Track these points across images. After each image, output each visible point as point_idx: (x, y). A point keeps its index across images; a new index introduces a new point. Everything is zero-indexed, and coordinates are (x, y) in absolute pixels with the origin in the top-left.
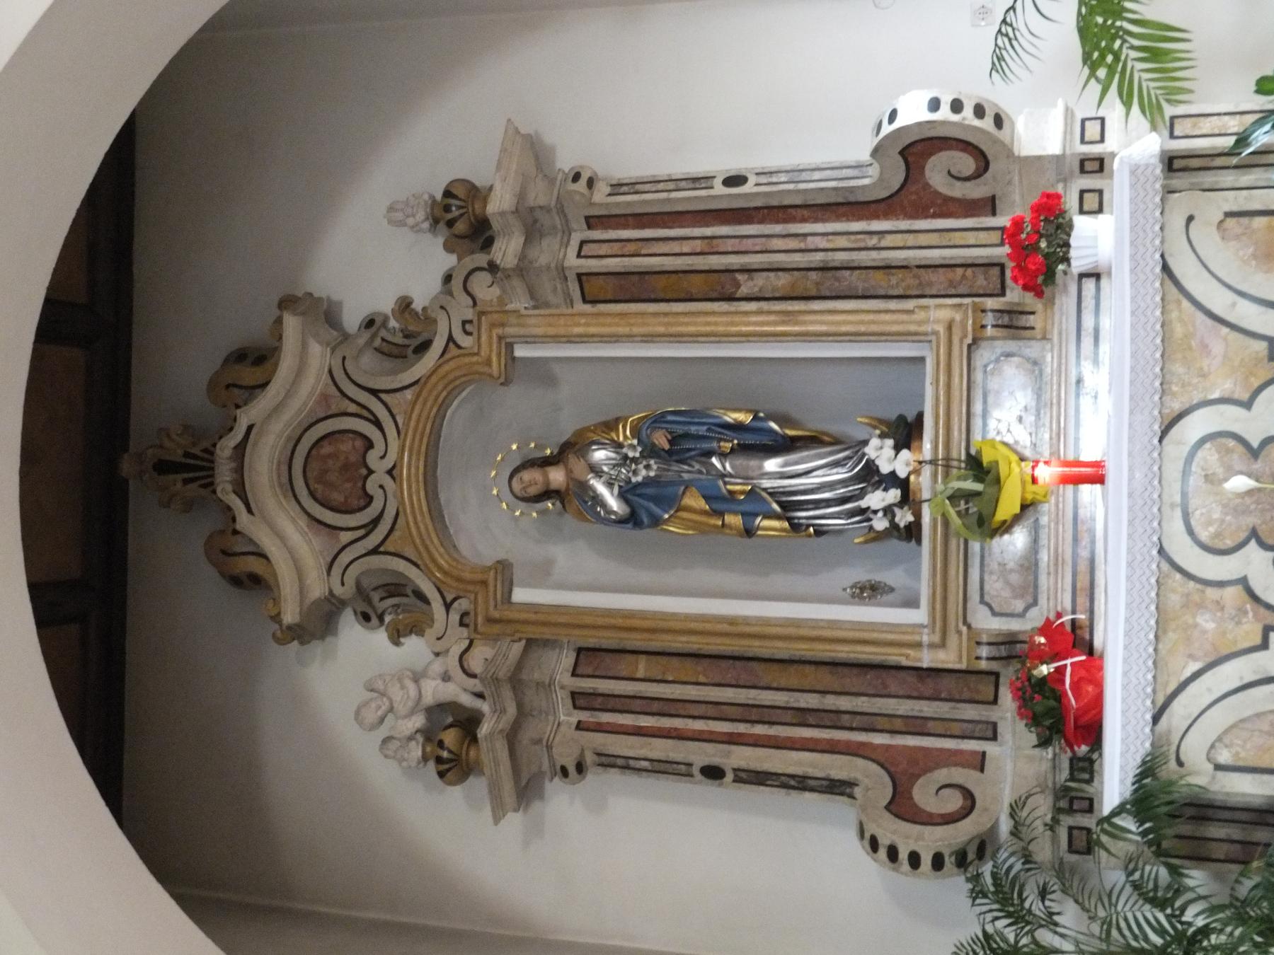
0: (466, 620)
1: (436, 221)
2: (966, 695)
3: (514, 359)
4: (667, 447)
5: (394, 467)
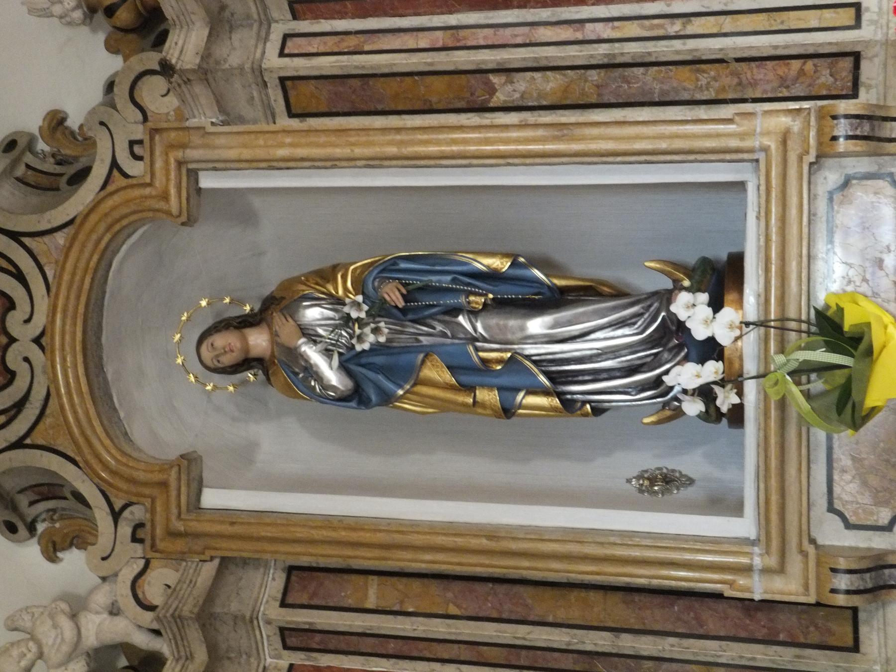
0: (140, 534)
2: (814, 638)
3: (199, 190)
4: (401, 304)
5: (42, 334)
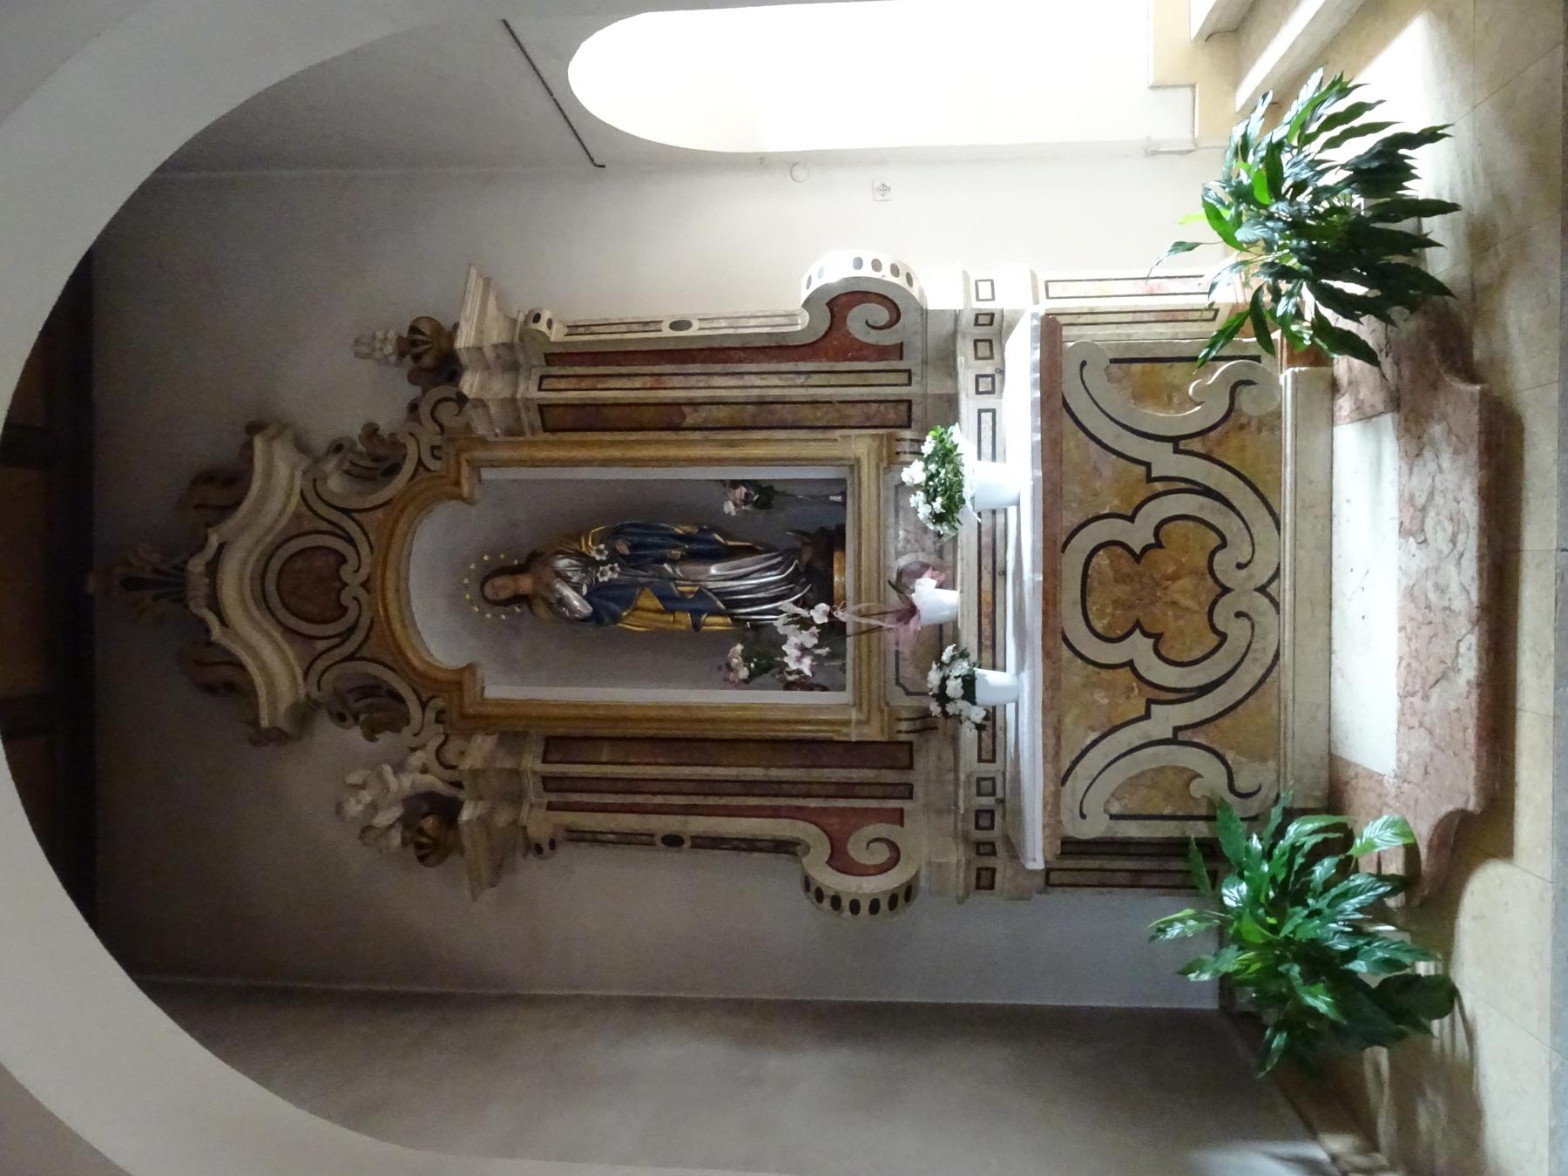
1: (402, 355)
4: (627, 552)
5: (368, 579)
